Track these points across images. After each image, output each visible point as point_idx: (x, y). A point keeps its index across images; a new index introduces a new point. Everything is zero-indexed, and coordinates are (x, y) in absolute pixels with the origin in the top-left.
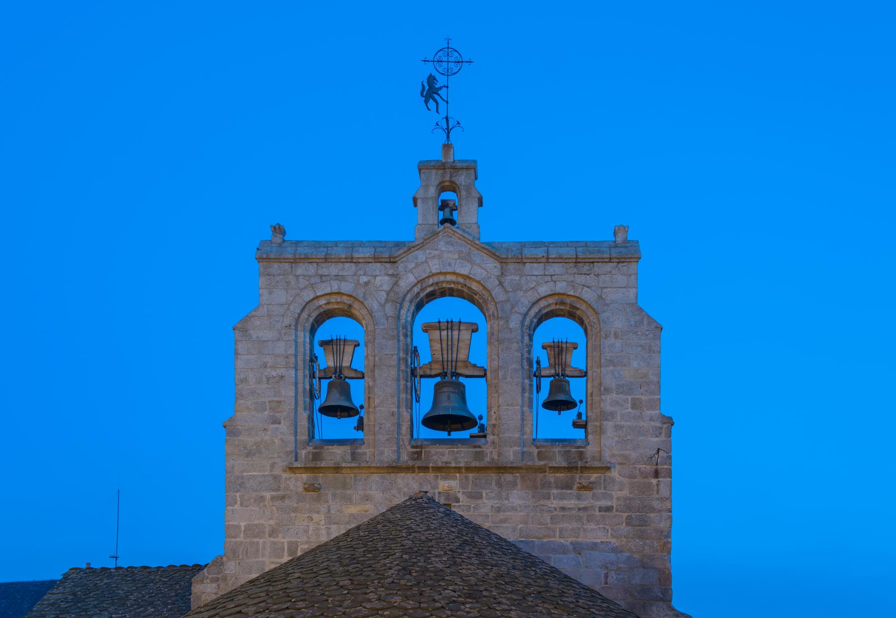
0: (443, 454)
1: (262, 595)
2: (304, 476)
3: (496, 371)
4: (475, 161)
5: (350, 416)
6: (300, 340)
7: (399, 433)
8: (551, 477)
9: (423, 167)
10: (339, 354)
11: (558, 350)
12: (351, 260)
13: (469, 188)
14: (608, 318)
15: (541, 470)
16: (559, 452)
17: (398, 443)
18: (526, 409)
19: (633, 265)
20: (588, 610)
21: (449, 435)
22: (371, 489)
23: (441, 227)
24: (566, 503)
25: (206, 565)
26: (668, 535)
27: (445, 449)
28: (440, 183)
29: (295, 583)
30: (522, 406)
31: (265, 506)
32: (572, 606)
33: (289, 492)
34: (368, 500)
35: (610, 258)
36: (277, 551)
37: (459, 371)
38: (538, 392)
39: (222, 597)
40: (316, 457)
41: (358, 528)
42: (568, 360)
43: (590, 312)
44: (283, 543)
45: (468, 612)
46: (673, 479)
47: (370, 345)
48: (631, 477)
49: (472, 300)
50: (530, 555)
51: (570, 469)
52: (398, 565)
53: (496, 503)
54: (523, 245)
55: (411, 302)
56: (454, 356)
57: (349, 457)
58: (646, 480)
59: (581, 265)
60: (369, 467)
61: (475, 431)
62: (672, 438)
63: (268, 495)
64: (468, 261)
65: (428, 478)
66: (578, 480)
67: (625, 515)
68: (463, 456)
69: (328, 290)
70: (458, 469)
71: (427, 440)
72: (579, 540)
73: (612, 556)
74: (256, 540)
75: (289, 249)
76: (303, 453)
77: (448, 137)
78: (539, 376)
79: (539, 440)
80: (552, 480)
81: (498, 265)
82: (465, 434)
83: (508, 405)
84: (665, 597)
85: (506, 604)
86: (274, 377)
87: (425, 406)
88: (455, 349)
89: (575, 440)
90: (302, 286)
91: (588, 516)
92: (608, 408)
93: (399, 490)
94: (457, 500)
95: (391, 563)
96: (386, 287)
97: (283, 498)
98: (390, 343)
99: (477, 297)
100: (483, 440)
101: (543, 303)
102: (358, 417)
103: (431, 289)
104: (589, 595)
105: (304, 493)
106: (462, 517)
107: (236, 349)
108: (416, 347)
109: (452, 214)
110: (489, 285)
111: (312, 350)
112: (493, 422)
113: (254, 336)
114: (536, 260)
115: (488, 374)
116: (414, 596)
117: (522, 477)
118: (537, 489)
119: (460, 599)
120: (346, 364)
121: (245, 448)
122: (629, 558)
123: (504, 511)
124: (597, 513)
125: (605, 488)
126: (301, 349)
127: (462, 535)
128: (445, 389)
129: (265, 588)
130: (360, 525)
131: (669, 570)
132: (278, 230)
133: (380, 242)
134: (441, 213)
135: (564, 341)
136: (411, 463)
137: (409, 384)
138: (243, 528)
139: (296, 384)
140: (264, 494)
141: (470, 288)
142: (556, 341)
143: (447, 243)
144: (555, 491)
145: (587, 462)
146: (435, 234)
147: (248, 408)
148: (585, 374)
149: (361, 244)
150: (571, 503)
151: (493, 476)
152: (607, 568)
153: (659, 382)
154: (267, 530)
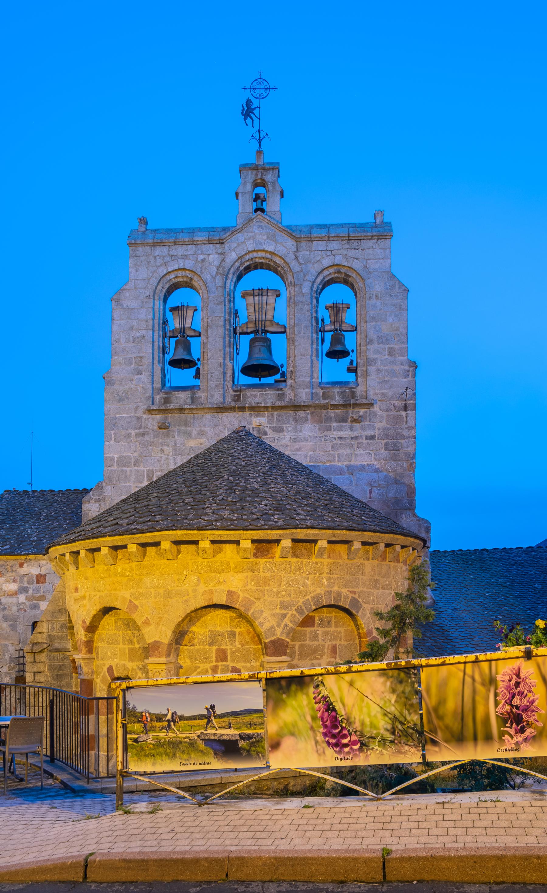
0: (255, 396)
1: (132, 510)
2: (158, 416)
3: (293, 327)
4: (278, 163)
5: (190, 367)
6: (156, 307)
7: (225, 380)
8: (332, 413)
9: (243, 168)
10: (183, 317)
11: (337, 310)
12: (192, 242)
13: (274, 184)
14: (371, 283)
15: (325, 407)
16: (338, 392)
17: (224, 388)
18: (314, 358)
19: (388, 241)
20: (360, 517)
21: (260, 380)
22: (204, 425)
23: (255, 215)
24: (343, 434)
25: (91, 489)
26: (413, 458)
27: (256, 392)
28: (255, 181)
29: (154, 500)
30: (312, 356)
31: (131, 441)
32: (349, 514)
33: (147, 430)
34: (204, 434)
35: (372, 236)
36: (139, 478)
37: (268, 328)
38: (322, 344)
39: (104, 512)
40: (167, 401)
41: (197, 457)
42: (344, 318)
43: (358, 279)
44: (143, 471)
45: (276, 522)
46: (417, 412)
47: (205, 310)
48: (388, 411)
49: (276, 272)
50: (319, 475)
51: (345, 406)
52: (226, 485)
53: (292, 435)
54: (312, 227)
55: (234, 274)
56: (264, 316)
57: (189, 401)
58: (398, 413)
59: (352, 241)
60: (204, 408)
61: (278, 377)
62: (417, 379)
63: (133, 432)
64: (273, 240)
65: (245, 416)
66: (351, 415)
67: (384, 442)
68: (268, 397)
69: (176, 267)
70: (266, 408)
71: (244, 385)
72: (352, 463)
73: (375, 476)
74: (125, 469)
75: (150, 236)
76: (157, 398)
77: (260, 145)
78: (323, 331)
79: (324, 383)
80: (333, 415)
81: (294, 243)
82: (270, 380)
83: (301, 355)
84: (411, 507)
85: (303, 515)
86: (138, 338)
87: (243, 359)
88: (264, 311)
89: (348, 383)
90: (158, 264)
91: (358, 443)
92: (372, 356)
93: (225, 426)
94: (266, 434)
95: (221, 484)
96: (216, 263)
97: (143, 435)
98: (219, 307)
99: (279, 269)
100: (284, 384)
101: (326, 273)
102: (195, 368)
103: (248, 263)
104: (361, 506)
105: (158, 430)
106: (270, 446)
107: (112, 316)
108: (236, 310)
109: (262, 205)
110: (288, 260)
111: (164, 315)
112: (291, 369)
113: (125, 305)
114: (321, 239)
115: (288, 330)
116: (238, 510)
117: (312, 413)
118: (322, 422)
119: (271, 512)
120: (188, 325)
121: (118, 395)
122: (386, 476)
123: (299, 442)
124: (365, 441)
125: (370, 421)
126: (157, 315)
127: (271, 461)
128: (257, 344)
129: (134, 505)
130: (198, 455)
131: (414, 484)
132: (143, 221)
133: (213, 228)
134: (255, 203)
135: (341, 302)
136: (233, 404)
137: (232, 340)
138: (116, 459)
139: (153, 342)
140: (130, 431)
141: (275, 262)
142: (335, 302)
143: (259, 227)
144: (335, 424)
145: (357, 400)
146: (251, 220)
147: (120, 363)
148: (355, 329)
149: (200, 230)
150: (346, 433)
151: (291, 413)
152: (371, 485)
153: (407, 334)
154: (133, 460)
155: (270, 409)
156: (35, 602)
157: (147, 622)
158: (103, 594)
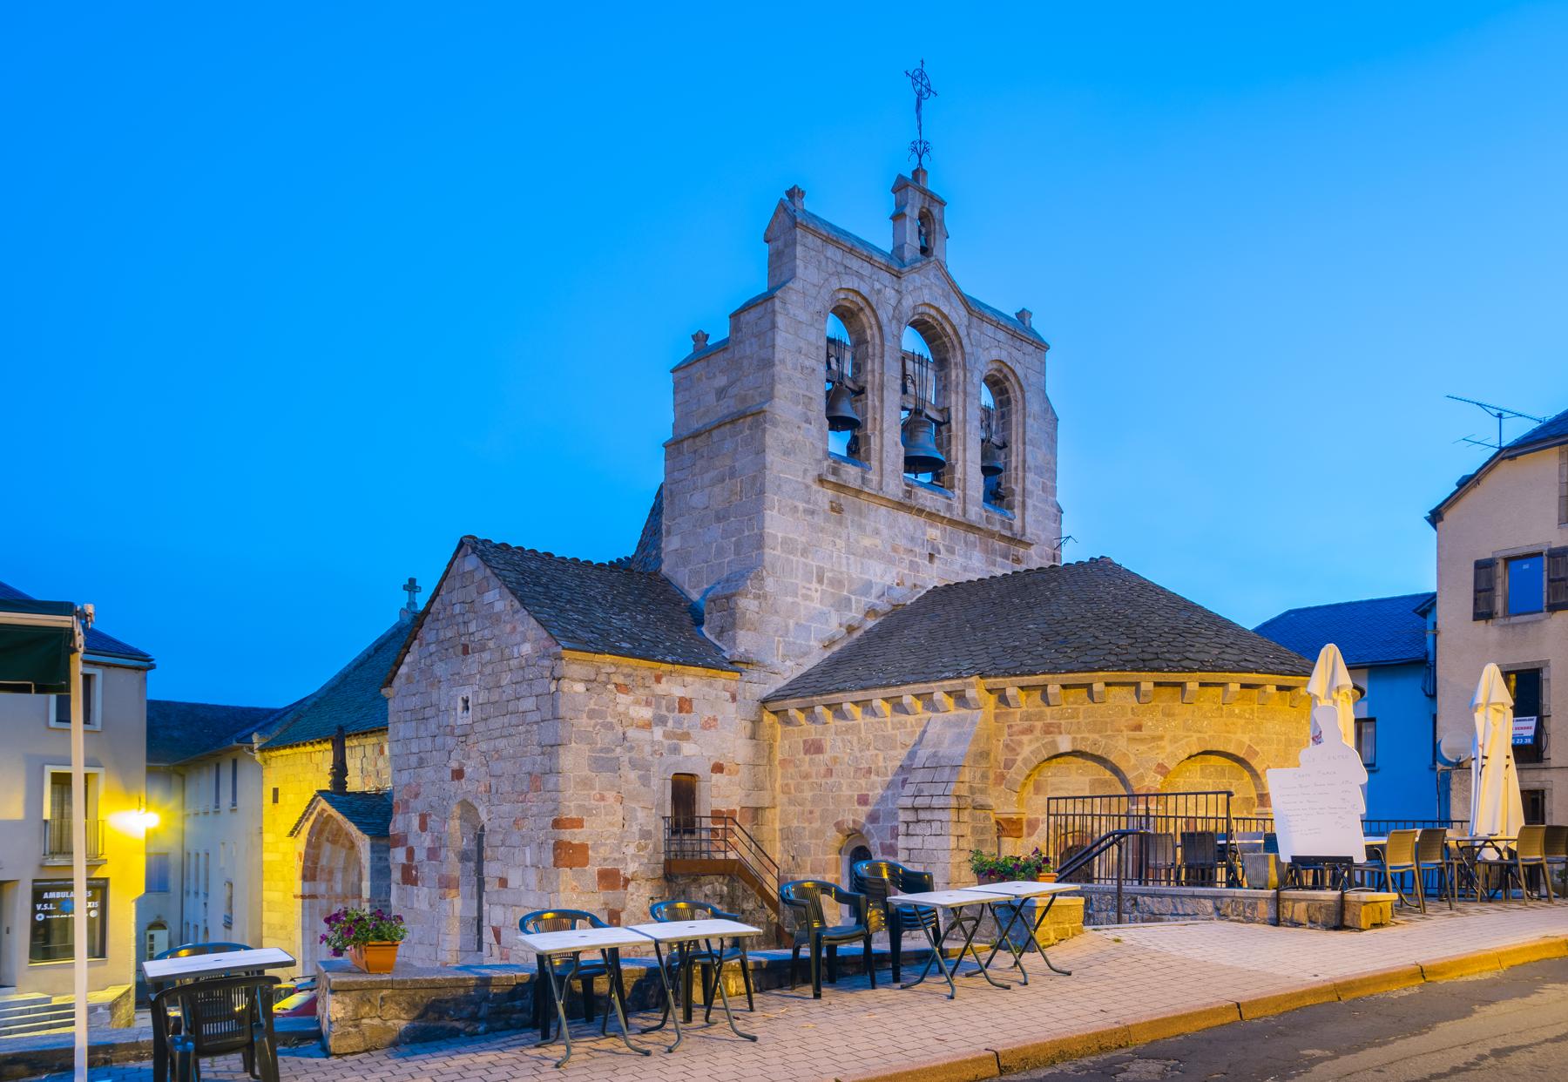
69: (850, 286)
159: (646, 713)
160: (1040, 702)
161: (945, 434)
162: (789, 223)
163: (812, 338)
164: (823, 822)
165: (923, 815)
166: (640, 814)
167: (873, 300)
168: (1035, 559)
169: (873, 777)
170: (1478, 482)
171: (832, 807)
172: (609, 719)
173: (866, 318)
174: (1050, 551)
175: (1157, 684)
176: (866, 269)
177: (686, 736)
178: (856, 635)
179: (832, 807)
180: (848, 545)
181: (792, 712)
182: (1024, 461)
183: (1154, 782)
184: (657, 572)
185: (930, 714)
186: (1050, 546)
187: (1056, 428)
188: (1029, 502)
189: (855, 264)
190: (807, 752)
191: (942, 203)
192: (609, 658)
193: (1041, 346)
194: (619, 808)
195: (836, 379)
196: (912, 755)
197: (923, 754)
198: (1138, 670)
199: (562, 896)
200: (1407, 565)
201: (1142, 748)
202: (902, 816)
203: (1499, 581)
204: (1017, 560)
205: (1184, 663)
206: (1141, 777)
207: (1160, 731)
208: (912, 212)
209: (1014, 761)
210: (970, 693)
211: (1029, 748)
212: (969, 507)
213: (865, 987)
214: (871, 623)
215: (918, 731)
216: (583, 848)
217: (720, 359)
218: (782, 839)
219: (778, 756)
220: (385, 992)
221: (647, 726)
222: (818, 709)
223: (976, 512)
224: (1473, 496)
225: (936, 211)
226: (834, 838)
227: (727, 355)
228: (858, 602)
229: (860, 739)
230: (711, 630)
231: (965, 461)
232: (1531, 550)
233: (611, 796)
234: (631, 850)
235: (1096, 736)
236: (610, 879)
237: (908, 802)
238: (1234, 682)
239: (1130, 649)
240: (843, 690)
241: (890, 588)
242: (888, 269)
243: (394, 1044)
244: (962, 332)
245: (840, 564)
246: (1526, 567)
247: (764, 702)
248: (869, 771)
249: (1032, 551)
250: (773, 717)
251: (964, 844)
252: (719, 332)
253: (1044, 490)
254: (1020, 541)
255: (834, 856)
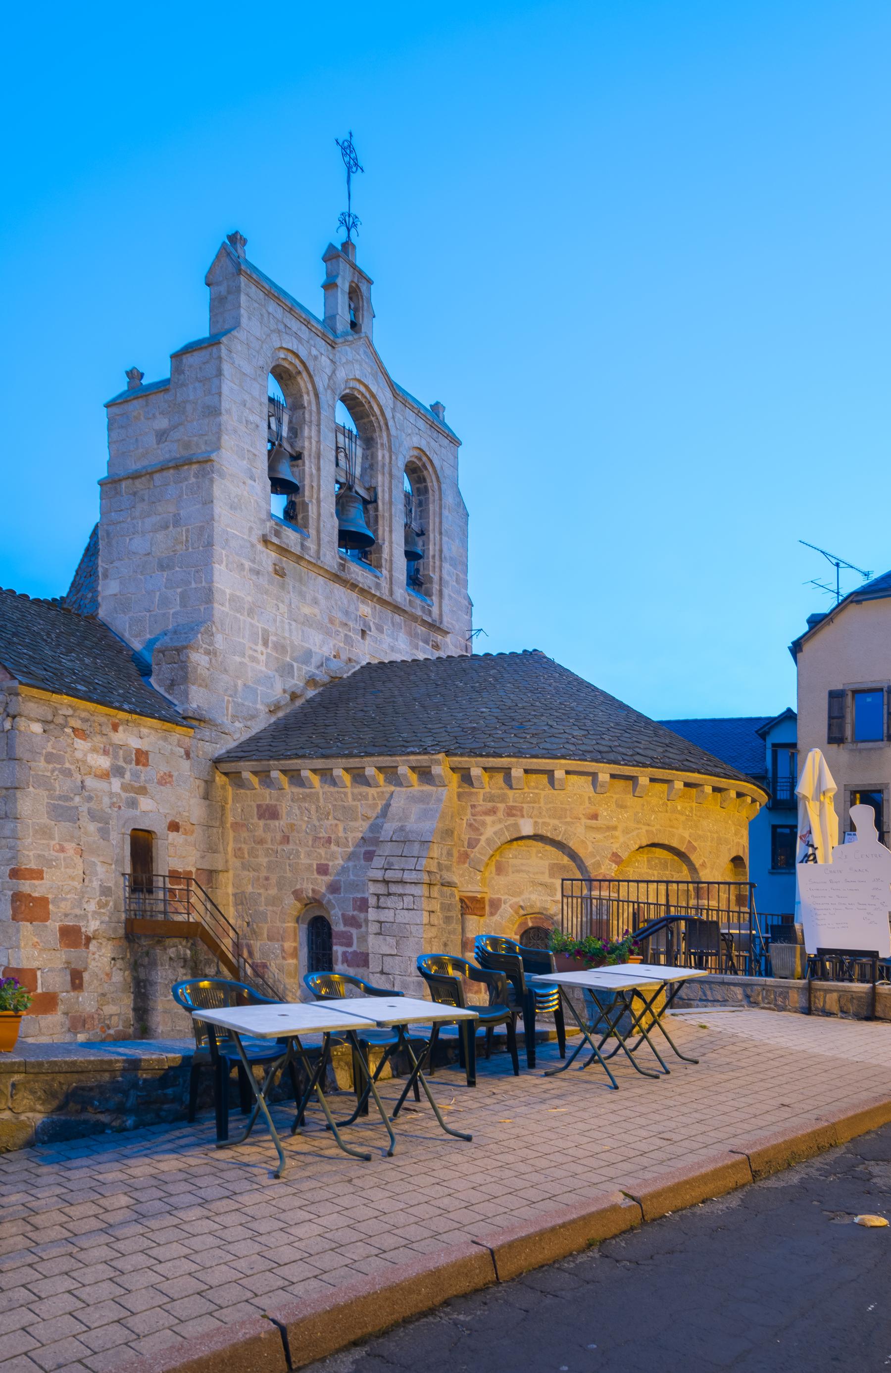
154: (246, 606)
155: (375, 600)
156: (133, 795)
157: (703, 865)
158: (654, 829)
159: (103, 762)
160: (503, 785)
161: (372, 512)
162: (231, 270)
163: (256, 393)
164: (280, 889)
165: (394, 888)
166: (100, 869)
167: (311, 365)
168: (451, 648)
169: (333, 847)
170: (832, 620)
171: (289, 875)
172: (67, 765)
173: (303, 382)
174: (463, 642)
175: (613, 776)
176: (304, 333)
177: (143, 791)
178: (299, 702)
179: (289, 875)
180: (290, 611)
181: (246, 775)
182: (441, 551)
183: (609, 869)
184: (94, 617)
185: (392, 788)
186: (463, 637)
187: (467, 524)
188: (446, 592)
189: (294, 325)
190: (261, 817)
191: (370, 282)
192: (66, 699)
193: (455, 442)
194: (78, 860)
195: (275, 441)
196: (375, 828)
197: (389, 828)
198: (597, 761)
199: (23, 953)
200: (766, 688)
201: (599, 836)
202: (372, 888)
203: (848, 710)
204: (436, 647)
205: (638, 758)
206: (598, 865)
207: (614, 822)
208: (344, 285)
209: (478, 841)
210: (436, 770)
211: (492, 829)
212: (395, 588)
213: (506, 1072)
214: (311, 693)
215: (380, 804)
216: (43, 902)
217: (159, 399)
218: (236, 904)
219: (230, 819)
220: (16, 1078)
221: (105, 776)
222: (275, 774)
223: (401, 594)
224: (827, 633)
225: (363, 287)
226: (292, 906)
227: (168, 397)
228: (300, 669)
229: (318, 808)
230: (160, 682)
231: (391, 543)
232: (874, 685)
233: (70, 847)
234: (92, 907)
235: (556, 822)
236: (71, 936)
237: (379, 875)
238: (679, 779)
239: (586, 741)
240: (303, 757)
241: (328, 659)
242: (324, 337)
243: (30, 1144)
244: (388, 414)
245: (283, 629)
246: (869, 700)
247: (217, 762)
248: (329, 841)
249: (449, 639)
250: (224, 778)
251: (435, 920)
252: (157, 370)
253: (457, 581)
254: (439, 628)
255: (291, 925)
